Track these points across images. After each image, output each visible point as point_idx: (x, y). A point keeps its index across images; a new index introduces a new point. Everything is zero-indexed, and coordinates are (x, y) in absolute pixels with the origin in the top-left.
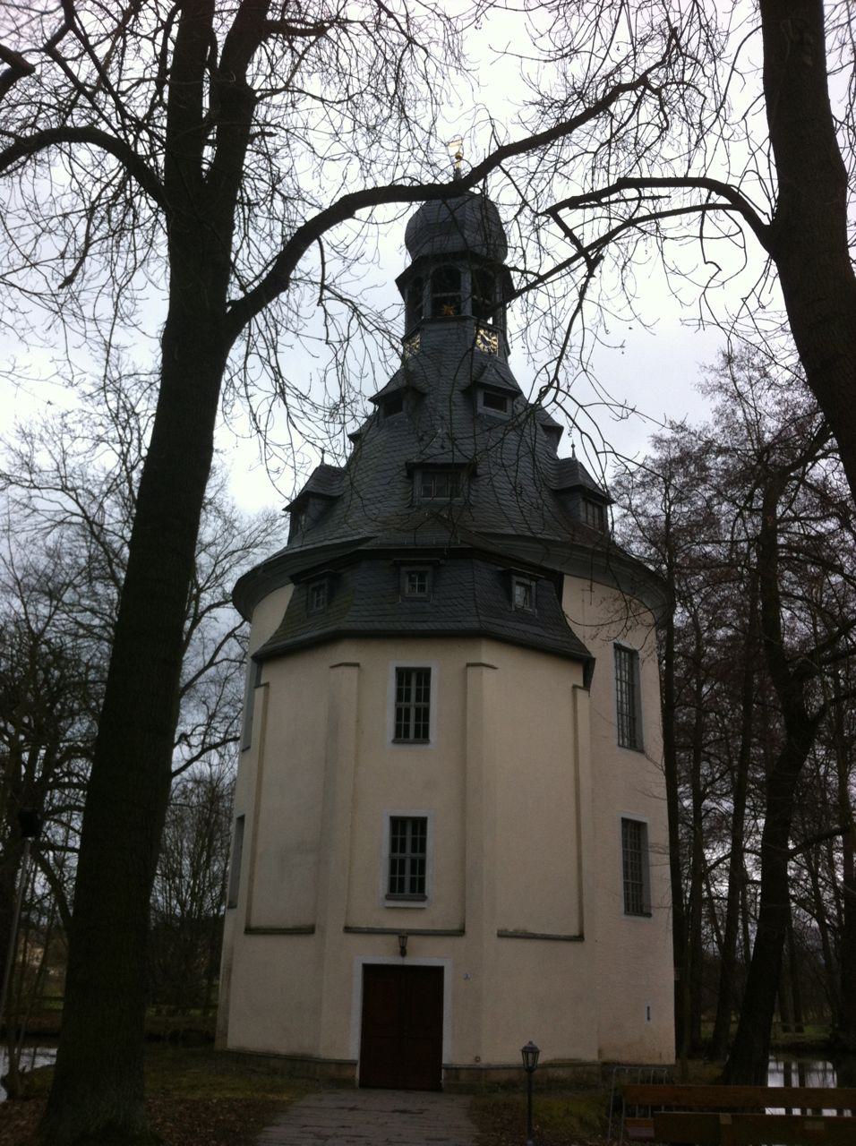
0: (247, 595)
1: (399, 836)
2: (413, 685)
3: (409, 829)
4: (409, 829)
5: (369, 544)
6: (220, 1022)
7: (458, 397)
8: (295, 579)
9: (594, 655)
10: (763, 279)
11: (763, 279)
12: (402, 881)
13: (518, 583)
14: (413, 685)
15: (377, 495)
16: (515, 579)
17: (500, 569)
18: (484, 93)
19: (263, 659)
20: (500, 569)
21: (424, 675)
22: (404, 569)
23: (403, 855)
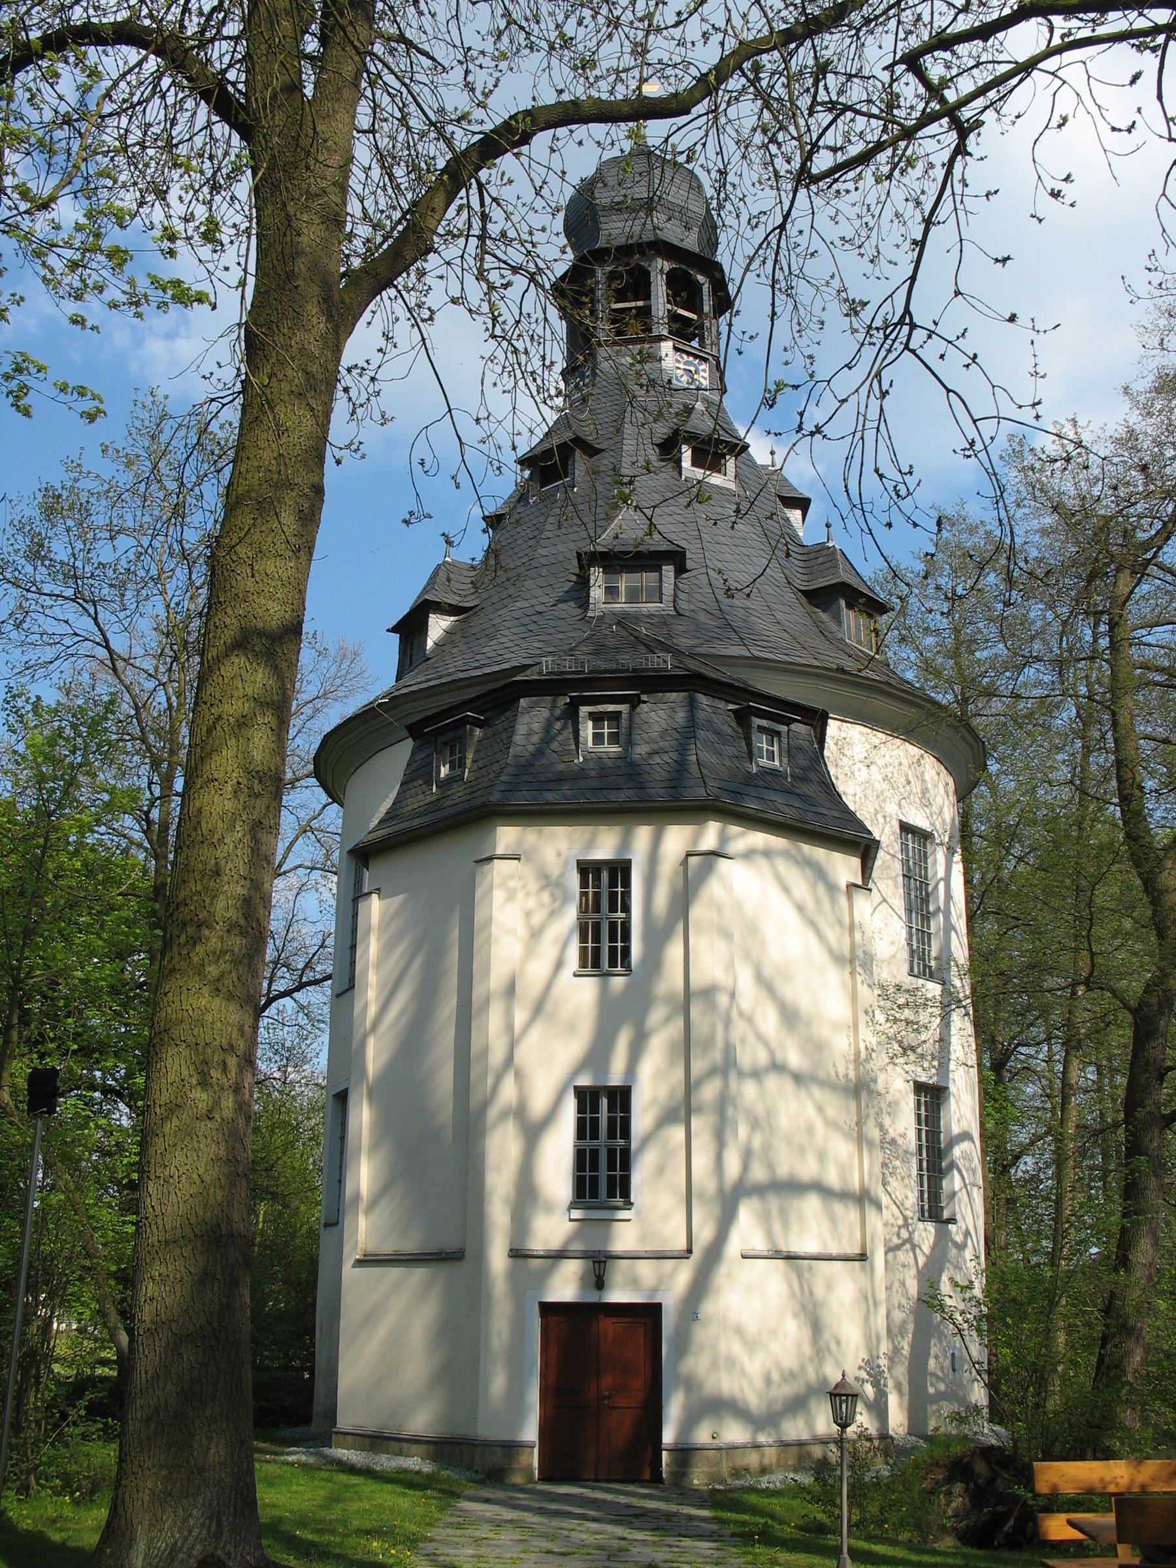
0: (337, 761)
1: (588, 1115)
2: (605, 883)
3: (604, 1103)
4: (604, 1103)
5: (528, 672)
6: (320, 1386)
7: (653, 455)
8: (414, 731)
9: (876, 835)
10: (988, 465)
11: (862, 411)
12: (594, 1181)
13: (761, 729)
14: (605, 883)
15: (533, 602)
16: (757, 721)
17: (731, 707)
18: (744, 8)
19: (363, 855)
20: (731, 707)
21: (620, 870)
22: (584, 710)
23: (595, 1142)
